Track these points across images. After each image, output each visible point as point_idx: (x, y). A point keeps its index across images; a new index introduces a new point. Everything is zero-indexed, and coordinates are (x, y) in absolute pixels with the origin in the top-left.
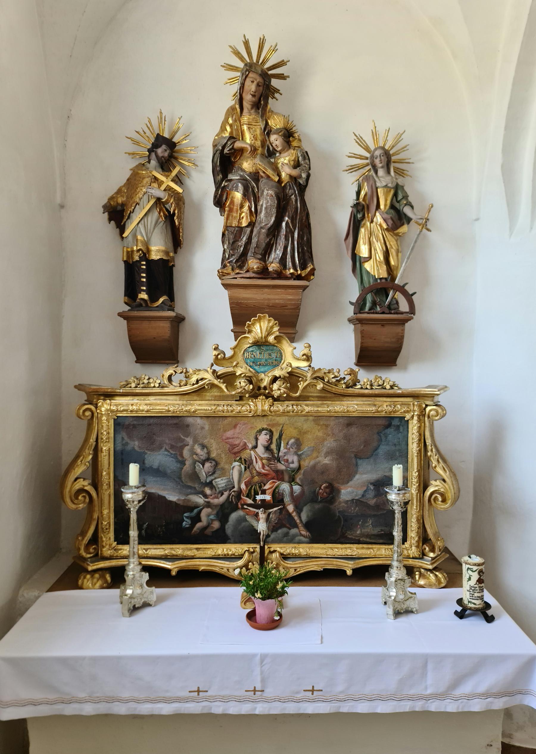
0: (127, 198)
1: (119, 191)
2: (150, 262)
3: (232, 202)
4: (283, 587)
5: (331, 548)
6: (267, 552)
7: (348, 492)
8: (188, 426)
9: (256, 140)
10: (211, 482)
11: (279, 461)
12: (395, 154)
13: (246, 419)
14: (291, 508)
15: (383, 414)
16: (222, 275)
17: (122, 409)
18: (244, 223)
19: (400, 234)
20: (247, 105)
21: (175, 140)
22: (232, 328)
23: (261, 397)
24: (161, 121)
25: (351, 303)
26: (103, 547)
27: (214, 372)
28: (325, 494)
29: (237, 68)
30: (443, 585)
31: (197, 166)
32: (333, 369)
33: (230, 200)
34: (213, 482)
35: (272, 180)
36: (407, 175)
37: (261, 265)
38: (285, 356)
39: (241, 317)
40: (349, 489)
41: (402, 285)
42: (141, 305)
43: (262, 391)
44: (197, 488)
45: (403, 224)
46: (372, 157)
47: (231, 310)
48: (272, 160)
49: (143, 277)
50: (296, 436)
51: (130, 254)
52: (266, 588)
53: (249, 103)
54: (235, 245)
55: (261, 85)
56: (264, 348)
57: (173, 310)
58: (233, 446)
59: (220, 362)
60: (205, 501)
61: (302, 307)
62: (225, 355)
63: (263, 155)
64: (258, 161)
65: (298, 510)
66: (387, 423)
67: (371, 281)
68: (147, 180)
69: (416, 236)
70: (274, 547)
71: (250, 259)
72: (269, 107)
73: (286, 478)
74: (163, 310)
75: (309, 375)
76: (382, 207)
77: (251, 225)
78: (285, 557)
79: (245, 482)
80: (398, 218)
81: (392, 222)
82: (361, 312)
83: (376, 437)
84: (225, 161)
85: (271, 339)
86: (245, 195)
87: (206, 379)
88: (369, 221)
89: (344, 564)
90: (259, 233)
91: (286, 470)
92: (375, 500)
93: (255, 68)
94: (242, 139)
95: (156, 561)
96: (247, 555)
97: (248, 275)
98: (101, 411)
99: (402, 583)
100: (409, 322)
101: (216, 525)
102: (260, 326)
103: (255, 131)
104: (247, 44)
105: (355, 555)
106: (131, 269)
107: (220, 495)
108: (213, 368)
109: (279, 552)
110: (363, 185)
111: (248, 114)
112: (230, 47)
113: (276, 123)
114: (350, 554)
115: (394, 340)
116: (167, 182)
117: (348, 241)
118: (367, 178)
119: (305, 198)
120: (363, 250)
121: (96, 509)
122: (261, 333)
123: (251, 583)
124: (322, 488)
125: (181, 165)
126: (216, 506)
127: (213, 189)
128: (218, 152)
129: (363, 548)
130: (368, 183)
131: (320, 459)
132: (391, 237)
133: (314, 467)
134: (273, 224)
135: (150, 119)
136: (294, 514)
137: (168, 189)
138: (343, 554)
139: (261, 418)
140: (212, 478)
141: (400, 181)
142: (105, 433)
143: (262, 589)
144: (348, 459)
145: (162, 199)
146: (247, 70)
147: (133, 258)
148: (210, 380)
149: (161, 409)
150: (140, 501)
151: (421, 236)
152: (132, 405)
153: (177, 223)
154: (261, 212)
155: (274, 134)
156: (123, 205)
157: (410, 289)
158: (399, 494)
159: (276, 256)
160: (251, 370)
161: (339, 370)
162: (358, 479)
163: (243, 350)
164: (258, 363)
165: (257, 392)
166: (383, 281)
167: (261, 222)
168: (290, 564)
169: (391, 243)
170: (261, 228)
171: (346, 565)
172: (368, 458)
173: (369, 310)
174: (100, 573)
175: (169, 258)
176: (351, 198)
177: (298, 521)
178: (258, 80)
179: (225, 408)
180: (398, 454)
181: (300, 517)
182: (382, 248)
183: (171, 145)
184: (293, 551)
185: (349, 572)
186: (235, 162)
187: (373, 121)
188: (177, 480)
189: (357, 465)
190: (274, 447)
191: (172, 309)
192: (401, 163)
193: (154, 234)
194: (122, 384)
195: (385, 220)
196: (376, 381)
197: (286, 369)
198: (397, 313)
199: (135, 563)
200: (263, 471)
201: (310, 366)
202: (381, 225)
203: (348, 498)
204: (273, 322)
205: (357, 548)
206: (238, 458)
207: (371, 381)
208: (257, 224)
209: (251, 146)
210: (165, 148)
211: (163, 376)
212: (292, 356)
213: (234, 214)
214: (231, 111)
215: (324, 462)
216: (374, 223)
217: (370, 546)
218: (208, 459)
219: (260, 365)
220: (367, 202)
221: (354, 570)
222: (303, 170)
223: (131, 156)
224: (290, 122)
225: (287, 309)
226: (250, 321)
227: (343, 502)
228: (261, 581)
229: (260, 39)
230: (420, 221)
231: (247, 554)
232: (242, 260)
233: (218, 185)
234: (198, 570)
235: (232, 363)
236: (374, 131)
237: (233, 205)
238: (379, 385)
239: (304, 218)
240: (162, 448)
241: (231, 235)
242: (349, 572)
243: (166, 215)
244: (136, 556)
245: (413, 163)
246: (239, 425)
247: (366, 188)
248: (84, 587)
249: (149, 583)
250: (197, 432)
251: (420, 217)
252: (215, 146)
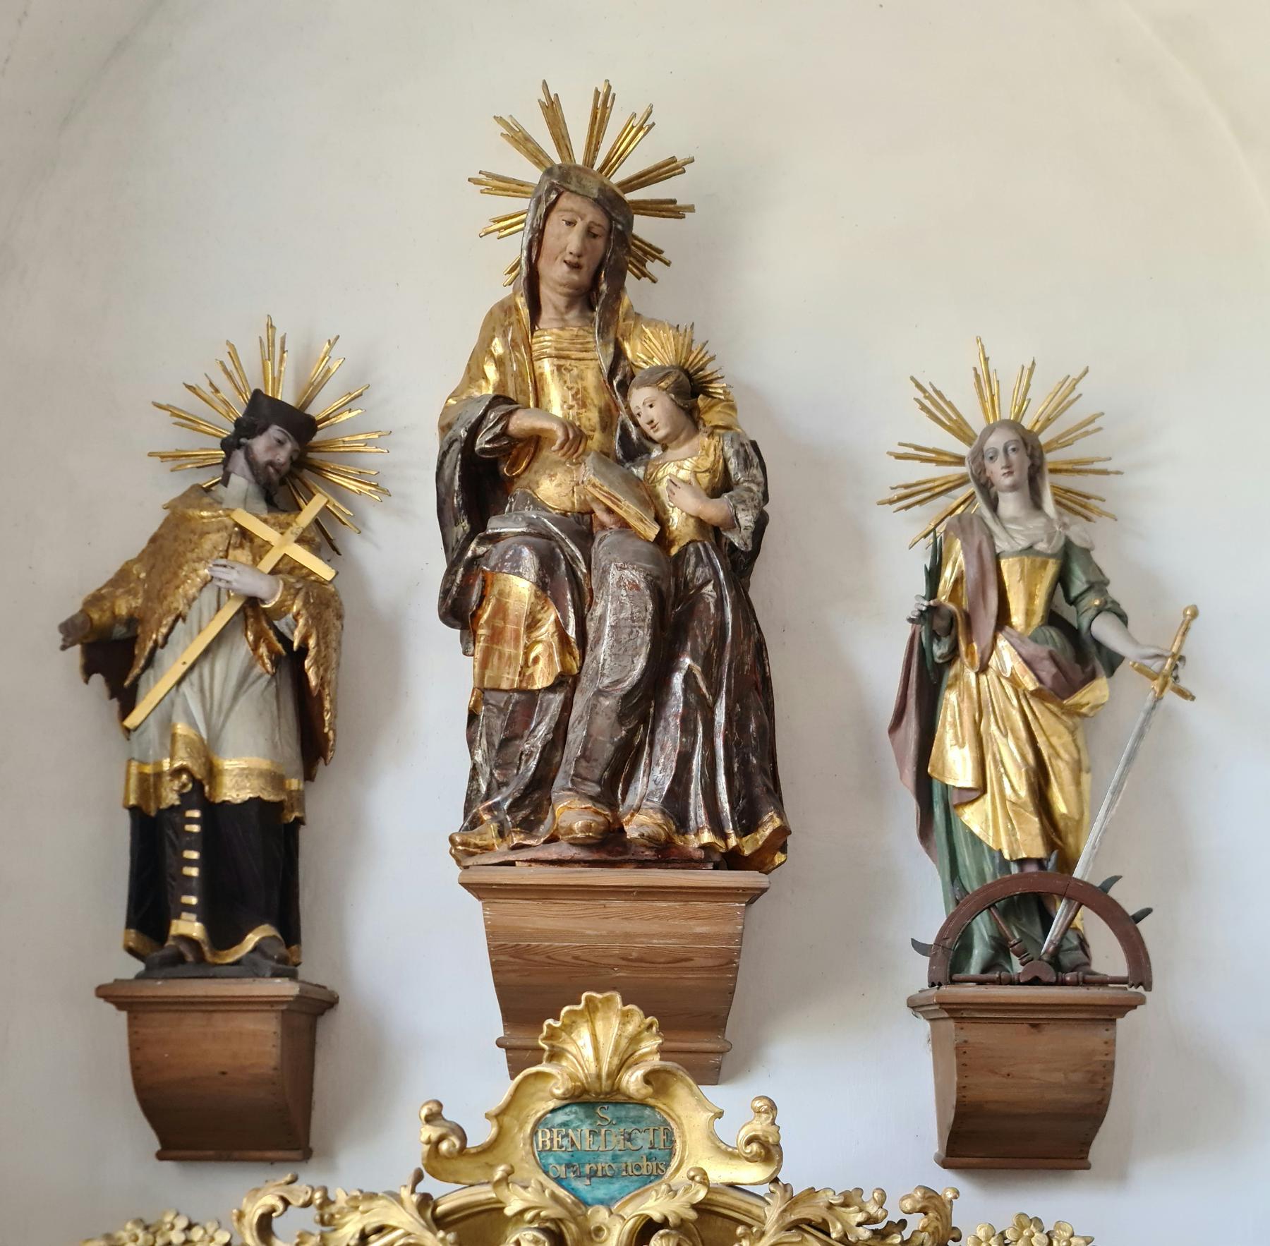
0: (148, 598)
1: (122, 578)
2: (216, 813)
3: (501, 610)
9: (584, 405)
12: (1062, 442)
16: (464, 851)
18: (542, 678)
19: (1084, 710)
20: (551, 296)
21: (316, 411)
22: (502, 1035)
24: (271, 357)
25: (919, 947)
27: (426, 1202)
29: (522, 184)
31: (387, 493)
32: (859, 1191)
33: (493, 601)
35: (637, 535)
36: (1101, 514)
37: (600, 819)
38: (684, 1143)
39: (532, 995)
41: (1098, 884)
42: (179, 959)
45: (1093, 677)
46: (979, 456)
47: (494, 972)
48: (639, 472)
49: (191, 863)
51: (150, 784)
53: (561, 289)
54: (511, 750)
55: (600, 239)
56: (608, 1113)
57: (292, 976)
59: (451, 1165)
61: (744, 964)
62: (463, 1138)
63: (607, 455)
64: (587, 472)
67: (988, 869)
68: (215, 539)
69: (1142, 716)
71: (560, 799)
72: (626, 301)
74: (256, 974)
75: (772, 1214)
76: (1017, 619)
77: (566, 682)
80: (1075, 657)
81: (1054, 670)
82: (956, 977)
84: (481, 477)
85: (632, 1081)
86: (545, 585)
87: (395, 1229)
88: (972, 666)
90: (592, 709)
93: (579, 182)
94: (537, 405)
97: (553, 852)
100: (1131, 1014)
102: (594, 1036)
103: (581, 377)
104: (552, 109)
106: (151, 834)
108: (421, 1188)
110: (949, 550)
111: (555, 324)
112: (499, 119)
113: (649, 350)
115: (1077, 1077)
116: (281, 546)
117: (901, 732)
118: (963, 526)
119: (751, 594)
120: (956, 765)
122: (597, 1059)
125: (335, 490)
127: (440, 565)
128: (457, 446)
130: (964, 541)
132: (1053, 719)
134: (640, 681)
135: (232, 346)
137: (286, 568)
141: (1078, 532)
145: (263, 601)
146: (552, 188)
147: (158, 798)
148: (408, 1234)
151: (1157, 717)
153: (313, 681)
154: (598, 641)
155: (644, 384)
156: (133, 621)
157: (1128, 899)
159: (651, 784)
160: (562, 1193)
161: (883, 1194)
163: (532, 1121)
164: (587, 1169)
166: (1032, 869)
167: (598, 674)
169: (1054, 740)
170: (600, 693)
173: (984, 971)
175: (283, 797)
176: (909, 592)
178: (589, 219)
182: (1023, 757)
183: (301, 425)
186: (511, 481)
187: (979, 340)
191: (287, 969)
192: (1079, 472)
193: (233, 716)
195: (1029, 663)
196: (1020, 1236)
197: (686, 1190)
198: (1086, 983)
201: (775, 1181)
202: (1014, 680)
204: (637, 1019)
207: (1002, 1233)
208: (584, 682)
209: (566, 425)
210: (280, 436)
211: (241, 1216)
212: (709, 1137)
213: (508, 650)
214: (502, 315)
216: (991, 674)
219: (593, 1174)
220: (965, 604)
222: (744, 502)
223: (170, 464)
224: (696, 347)
225: (692, 969)
226: (557, 1018)
229: (597, 93)
230: (1155, 666)
232: (533, 802)
233: (455, 553)
235: (492, 1167)
236: (981, 370)
237: (504, 619)
239: (749, 659)
241: (499, 718)
243: (278, 654)
245: (1118, 473)
247: (961, 558)
251: (1153, 651)
252: (445, 428)
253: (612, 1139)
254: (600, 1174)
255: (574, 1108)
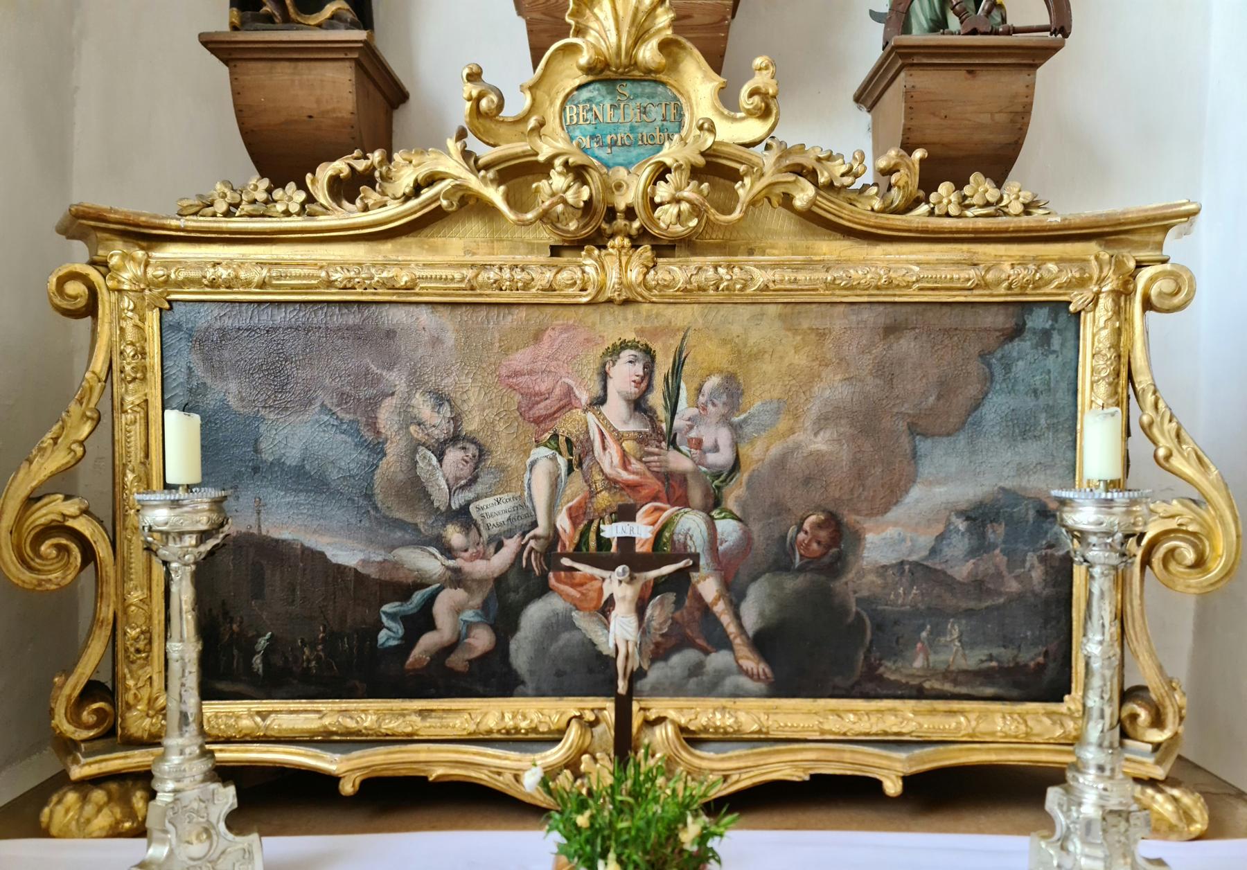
4: (703, 838)
5: (838, 713)
6: (636, 721)
7: (883, 542)
8: (390, 334)
10: (464, 510)
11: (673, 443)
13: (571, 312)
14: (709, 588)
15: (1000, 294)
17: (182, 275)
23: (618, 241)
25: (875, 16)
26: (129, 707)
28: (815, 546)
30: (1198, 827)
34: (472, 508)
40: (891, 532)
43: (620, 222)
44: (421, 526)
50: (725, 365)
52: (638, 839)
56: (627, 89)
58: (533, 398)
60: (448, 568)
62: (500, 106)
65: (734, 594)
66: (1011, 324)
70: (658, 707)
73: (696, 495)
78: (692, 739)
79: (570, 508)
83: (975, 367)
85: (648, 53)
89: (878, 762)
91: (696, 473)
92: (970, 564)
95: (293, 749)
96: (574, 732)
98: (119, 282)
99: (1123, 825)
101: (482, 640)
105: (909, 734)
107: (492, 549)
109: (673, 722)
114: (895, 729)
121: (110, 589)
123: (582, 820)
124: (806, 526)
126: (481, 582)
129: (933, 712)
131: (799, 436)
133: (781, 464)
136: (720, 608)
138: (874, 730)
139: (617, 310)
140: (468, 495)
142: (129, 351)
143: (625, 844)
144: (890, 438)
149: (305, 277)
150: (203, 536)
152: (215, 265)
158: (1108, 503)
162: (917, 501)
165: (604, 226)
168: (710, 759)
171: (885, 763)
172: (949, 435)
174: (113, 786)
177: (732, 629)
179: (506, 274)
180: (1043, 421)
181: (737, 617)
184: (718, 720)
185: (892, 787)
188: (362, 502)
189: (914, 455)
190: (656, 399)
194: (185, 203)
199: (188, 751)
200: (625, 476)
203: (889, 557)
205: (915, 713)
206: (547, 436)
215: (813, 447)
217: (955, 705)
218: (455, 438)
219: (614, 144)
221: (908, 781)
227: (870, 571)
228: (620, 812)
231: (574, 727)
234: (426, 778)
238: (988, 204)
240: (310, 402)
242: (892, 787)
244: (193, 728)
246: (549, 332)
248: (54, 831)
249: (236, 822)
250: (420, 352)
253: (629, 111)
254: (619, 143)
255: (597, 86)
